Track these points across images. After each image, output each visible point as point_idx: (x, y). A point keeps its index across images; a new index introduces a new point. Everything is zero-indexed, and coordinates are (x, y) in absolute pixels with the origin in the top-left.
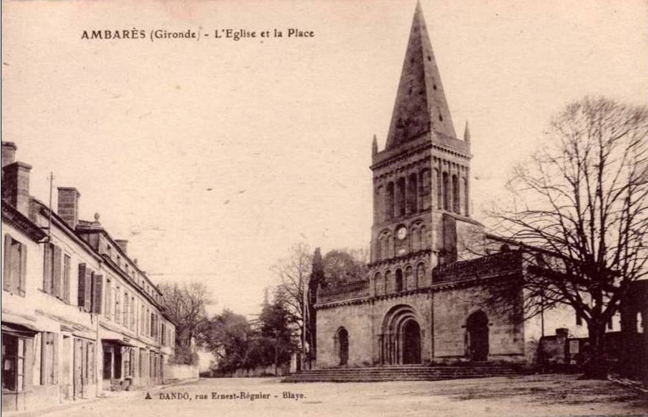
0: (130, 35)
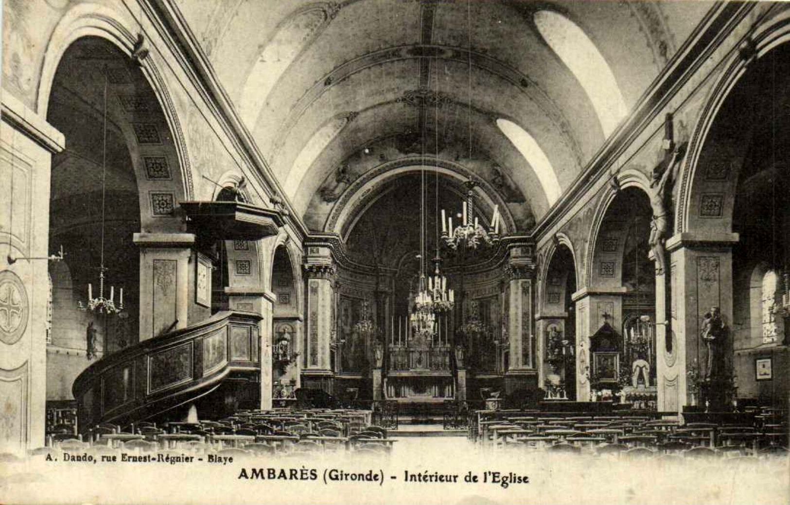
0: (299, 475)
